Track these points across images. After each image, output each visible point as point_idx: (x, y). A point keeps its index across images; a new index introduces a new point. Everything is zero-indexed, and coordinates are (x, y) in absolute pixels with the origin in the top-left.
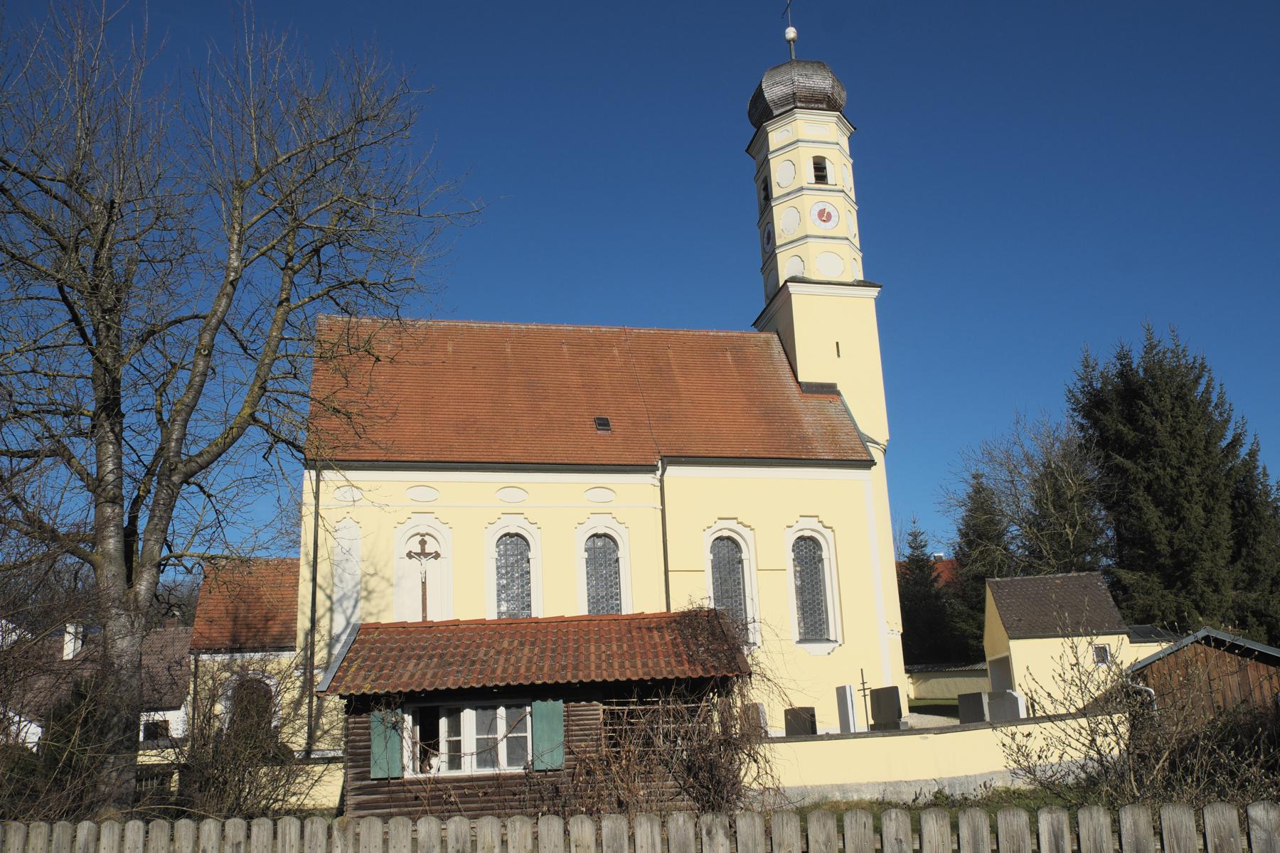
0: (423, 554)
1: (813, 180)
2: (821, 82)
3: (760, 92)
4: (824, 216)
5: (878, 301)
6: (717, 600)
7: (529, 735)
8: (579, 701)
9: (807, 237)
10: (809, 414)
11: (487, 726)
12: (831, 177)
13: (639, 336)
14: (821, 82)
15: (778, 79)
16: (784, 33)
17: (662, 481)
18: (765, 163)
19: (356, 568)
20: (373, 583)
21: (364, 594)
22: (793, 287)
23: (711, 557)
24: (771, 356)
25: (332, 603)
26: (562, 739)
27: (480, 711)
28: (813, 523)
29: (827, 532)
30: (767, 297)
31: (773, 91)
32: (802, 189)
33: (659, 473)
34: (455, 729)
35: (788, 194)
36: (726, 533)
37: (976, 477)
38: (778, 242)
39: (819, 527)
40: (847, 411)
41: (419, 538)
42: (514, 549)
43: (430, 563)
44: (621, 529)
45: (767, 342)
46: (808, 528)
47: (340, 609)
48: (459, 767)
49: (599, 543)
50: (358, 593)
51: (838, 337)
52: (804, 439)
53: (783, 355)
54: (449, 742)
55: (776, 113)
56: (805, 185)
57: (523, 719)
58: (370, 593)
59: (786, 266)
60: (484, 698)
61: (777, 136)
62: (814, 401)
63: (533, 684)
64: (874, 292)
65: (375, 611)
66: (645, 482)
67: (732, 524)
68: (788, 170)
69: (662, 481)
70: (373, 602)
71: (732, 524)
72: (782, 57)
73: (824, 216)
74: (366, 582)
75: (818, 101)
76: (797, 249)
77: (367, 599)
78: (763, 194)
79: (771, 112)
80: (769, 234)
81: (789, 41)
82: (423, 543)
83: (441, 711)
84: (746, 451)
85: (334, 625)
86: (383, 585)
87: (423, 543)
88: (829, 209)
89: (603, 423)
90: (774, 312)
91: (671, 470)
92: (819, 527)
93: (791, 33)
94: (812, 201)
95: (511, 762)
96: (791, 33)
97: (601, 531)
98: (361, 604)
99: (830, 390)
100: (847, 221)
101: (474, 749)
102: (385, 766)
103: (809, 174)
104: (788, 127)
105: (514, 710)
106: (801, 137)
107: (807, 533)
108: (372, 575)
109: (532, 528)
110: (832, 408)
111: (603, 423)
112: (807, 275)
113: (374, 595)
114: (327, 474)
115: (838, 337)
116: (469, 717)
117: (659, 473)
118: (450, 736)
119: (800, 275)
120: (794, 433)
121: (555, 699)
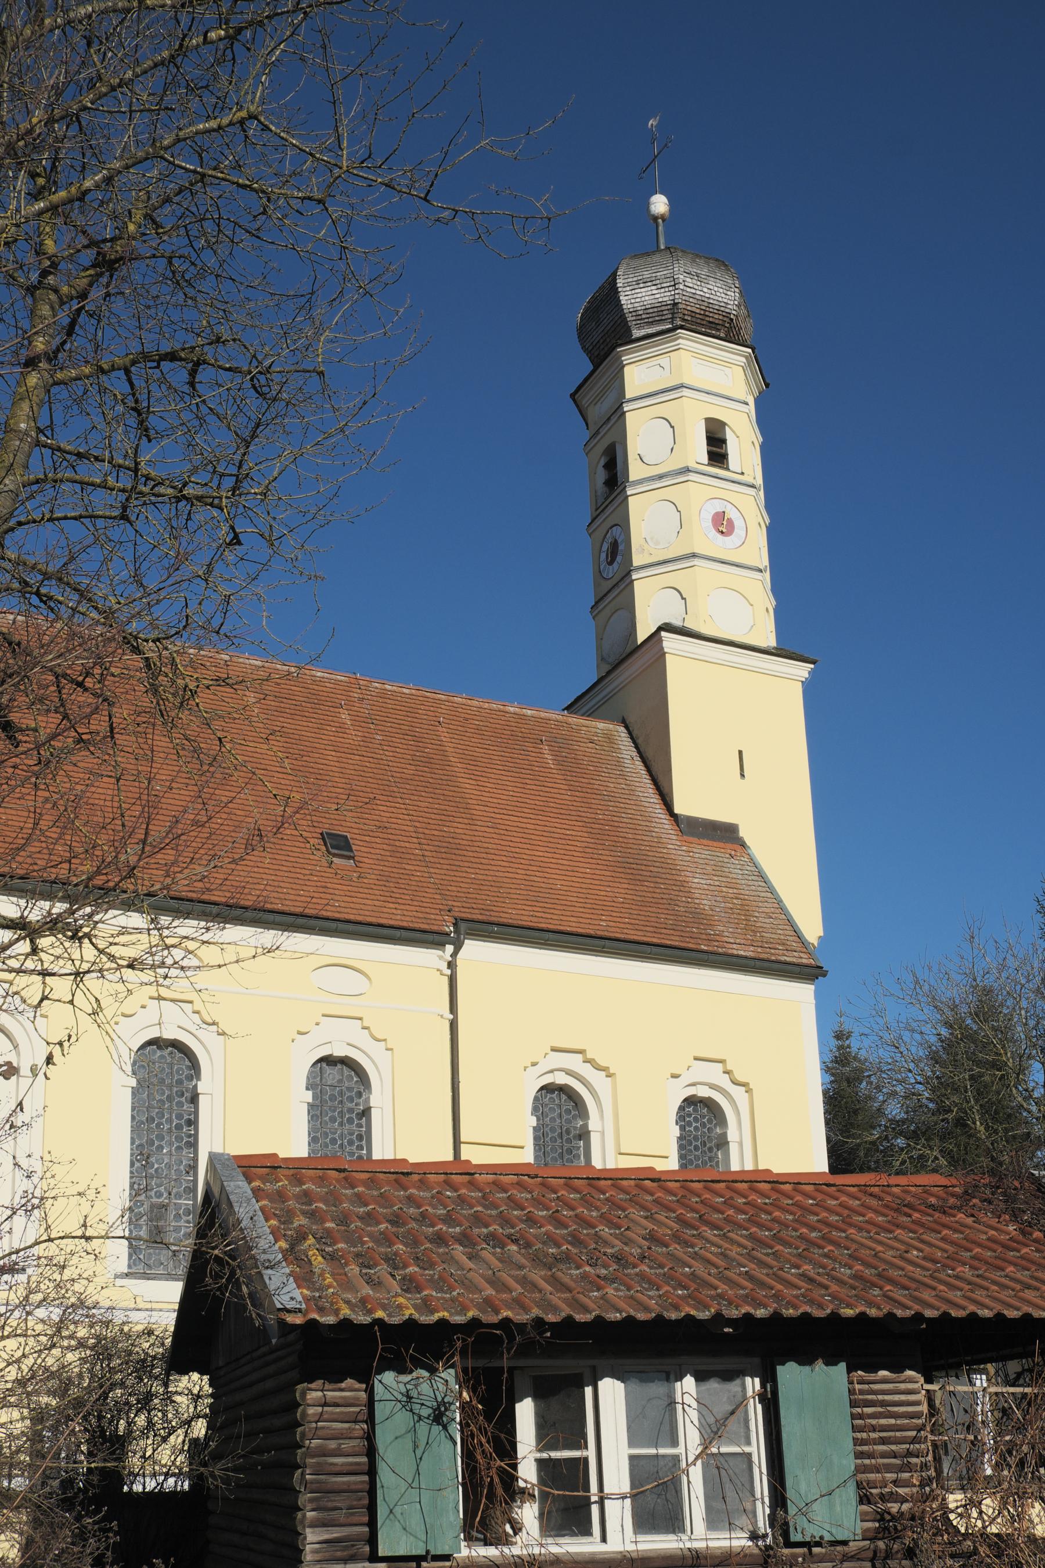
1: (705, 459)
2: (721, 292)
3: (609, 293)
4: (722, 524)
5: (809, 688)
7: (591, 1453)
8: (874, 1369)
9: (694, 555)
10: (697, 867)
11: (654, 1424)
12: (734, 459)
13: (383, 694)
14: (721, 292)
15: (646, 275)
16: (647, 205)
17: (451, 965)
18: (617, 415)
22: (670, 642)
23: (533, 1121)
24: (619, 763)
26: (850, 1463)
27: (635, 1386)
28: (714, 1074)
29: (738, 1092)
30: (602, 659)
31: (637, 295)
32: (687, 470)
33: (450, 949)
34: (565, 1425)
35: (661, 477)
36: (561, 1079)
37: (839, 1036)
38: (637, 560)
39: (724, 1082)
40: (762, 876)
42: (167, 1075)
44: (376, 1050)
45: (610, 738)
46: (705, 1079)
49: (332, 1074)
51: (741, 742)
52: (698, 916)
53: (639, 764)
54: (540, 1462)
55: (637, 333)
56: (692, 465)
57: (741, 1404)
59: (651, 605)
60: (652, 1348)
61: (640, 372)
62: (703, 852)
63: (834, 1317)
64: (803, 670)
66: (425, 962)
67: (574, 1062)
68: (653, 439)
69: (451, 965)
71: (574, 1062)
72: (647, 242)
73: (722, 524)
75: (713, 325)
76: (678, 577)
78: (601, 475)
79: (628, 331)
80: (615, 545)
81: (655, 218)
83: (521, 1381)
84: (603, 926)
86: (954, 975)
88: (732, 514)
89: (338, 844)
90: (624, 680)
91: (472, 948)
92: (724, 1082)
93: (659, 204)
94: (704, 495)
95: (713, 1521)
96: (659, 204)
97: (339, 1052)
99: (724, 834)
100: (752, 542)
101: (626, 1488)
102: (415, 1523)
103: (698, 451)
104: (664, 361)
105: (714, 1385)
106: (686, 381)
107: (703, 1092)
110: (735, 868)
111: (338, 844)
112: (690, 624)
115: (741, 742)
116: (611, 1398)
117: (450, 949)
118: (631, 1444)
119: (677, 623)
120: (669, 907)
121: (830, 1362)
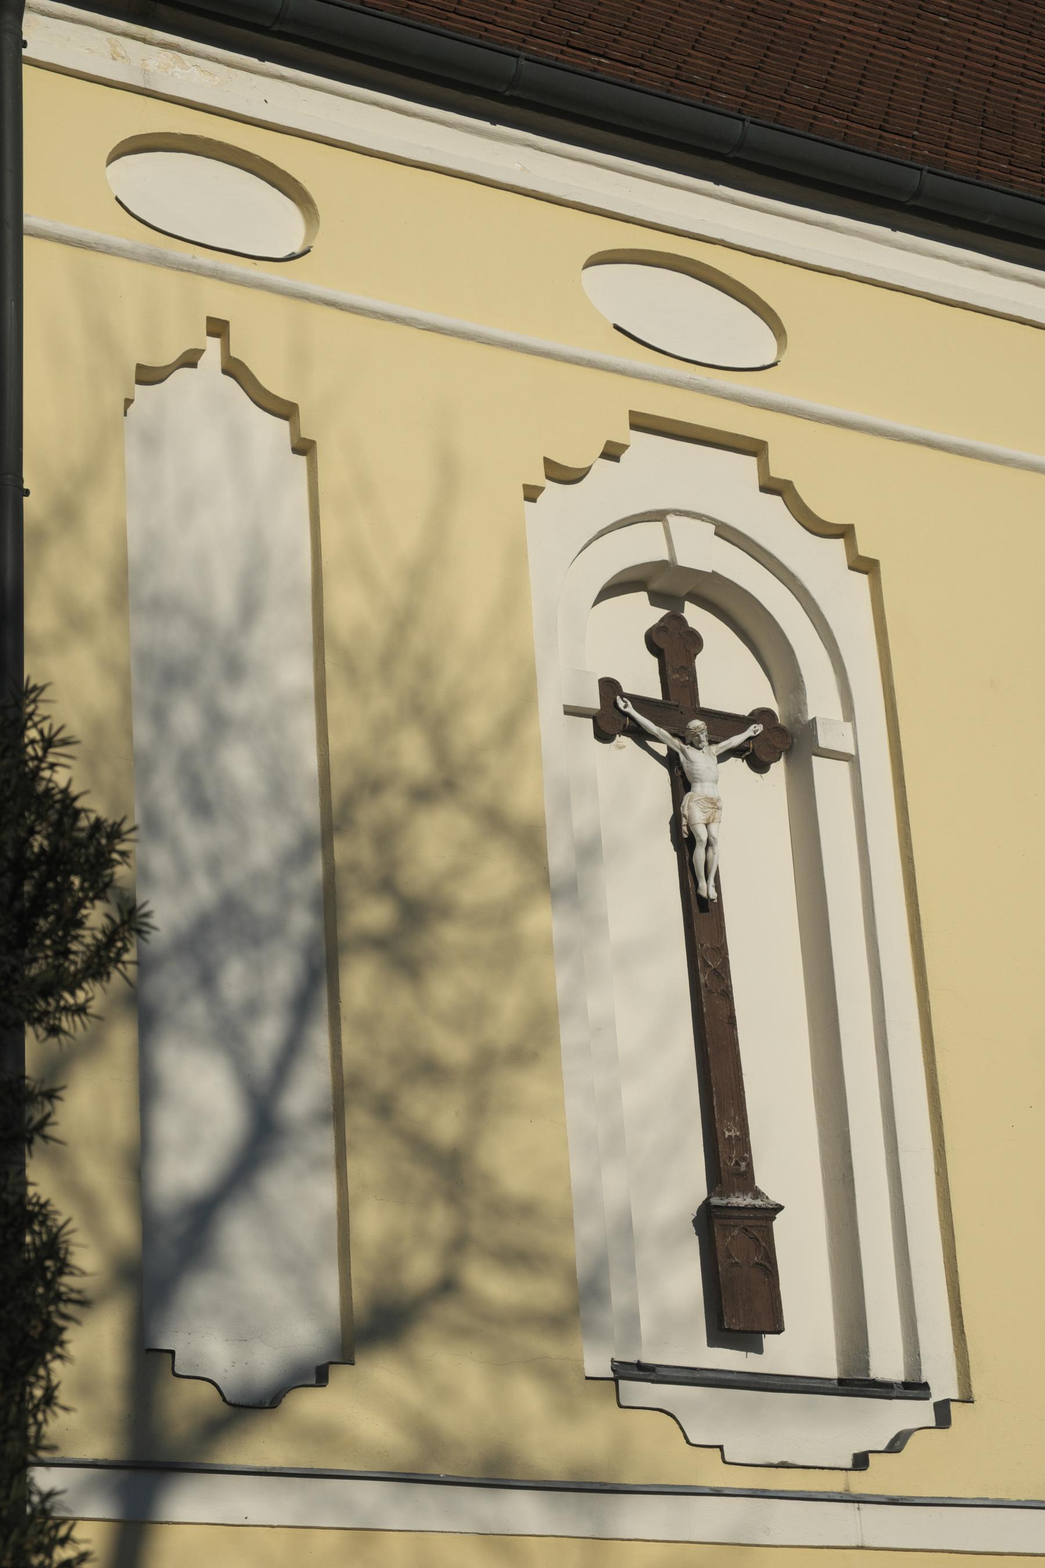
20: (435, 842)
47: (197, 1010)
58: (417, 913)
65: (454, 1049)
70: (446, 989)
85: (168, 1126)
108: (423, 795)
113: (451, 935)
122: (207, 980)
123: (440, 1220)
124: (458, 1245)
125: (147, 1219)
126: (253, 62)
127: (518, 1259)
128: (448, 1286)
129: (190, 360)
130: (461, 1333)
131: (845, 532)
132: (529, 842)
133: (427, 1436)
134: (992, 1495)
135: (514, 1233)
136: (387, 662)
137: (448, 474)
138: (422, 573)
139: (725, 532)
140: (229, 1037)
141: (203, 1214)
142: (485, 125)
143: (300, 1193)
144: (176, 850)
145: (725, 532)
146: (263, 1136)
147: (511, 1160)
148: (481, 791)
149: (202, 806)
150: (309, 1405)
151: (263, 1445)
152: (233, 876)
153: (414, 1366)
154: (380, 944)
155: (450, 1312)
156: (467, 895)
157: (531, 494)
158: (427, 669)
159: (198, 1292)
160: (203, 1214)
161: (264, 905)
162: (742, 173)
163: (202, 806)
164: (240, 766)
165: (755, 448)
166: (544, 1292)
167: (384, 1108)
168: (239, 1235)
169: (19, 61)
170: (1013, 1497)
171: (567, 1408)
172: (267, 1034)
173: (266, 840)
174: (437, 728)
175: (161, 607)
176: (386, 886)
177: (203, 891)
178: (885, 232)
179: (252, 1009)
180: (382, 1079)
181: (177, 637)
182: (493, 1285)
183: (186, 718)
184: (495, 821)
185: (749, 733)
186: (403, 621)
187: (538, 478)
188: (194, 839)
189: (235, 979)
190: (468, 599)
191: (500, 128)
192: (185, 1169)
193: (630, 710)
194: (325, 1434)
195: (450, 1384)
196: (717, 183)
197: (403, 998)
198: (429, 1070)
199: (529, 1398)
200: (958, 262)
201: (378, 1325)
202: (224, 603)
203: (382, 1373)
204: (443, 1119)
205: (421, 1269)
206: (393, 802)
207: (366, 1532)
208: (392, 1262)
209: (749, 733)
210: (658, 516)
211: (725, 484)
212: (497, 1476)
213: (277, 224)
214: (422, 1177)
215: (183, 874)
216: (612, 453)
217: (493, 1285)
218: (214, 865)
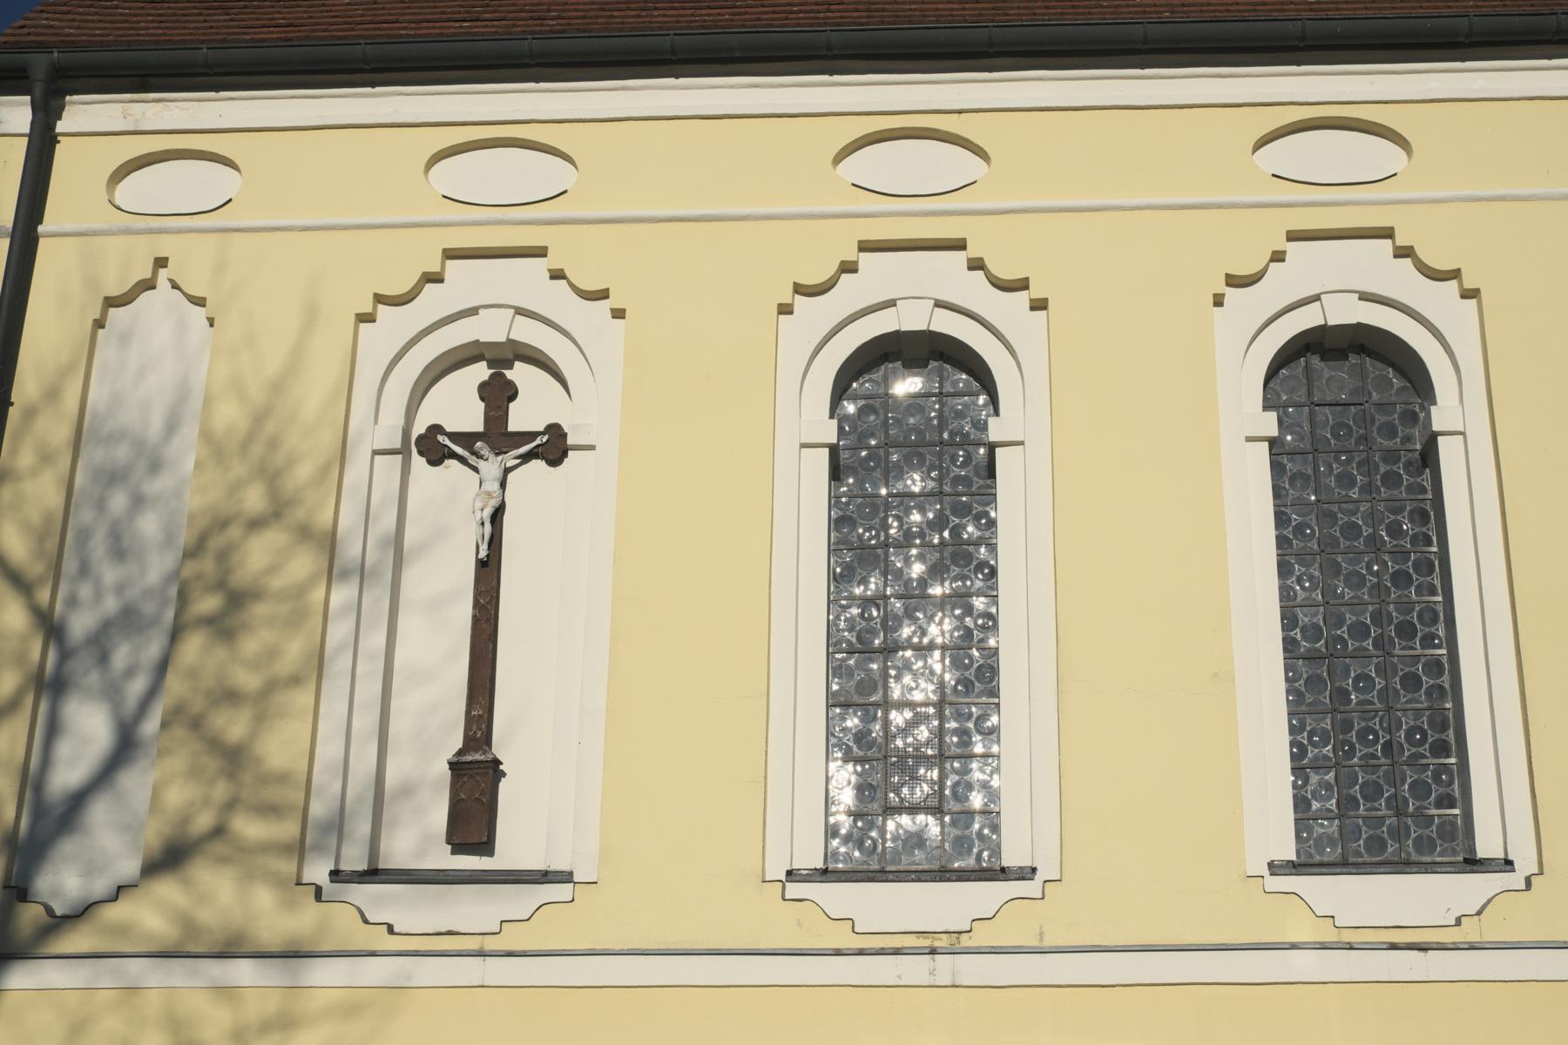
0: (496, 435)
6: (1298, 855)
19: (187, 485)
20: (257, 554)
21: (208, 604)
25: (65, 655)
41: (481, 371)
43: (532, 481)
47: (94, 678)
48: (485, 846)
49: (1336, 378)
50: (183, 598)
58: (238, 599)
65: (248, 680)
70: (250, 645)
74: (224, 556)
77: (223, 627)
82: (498, 394)
85: (64, 749)
87: (498, 394)
98: (193, 648)
108: (255, 524)
109: (1008, 310)
113: (260, 610)
114: (84, 114)
122: (104, 658)
123: (221, 791)
124: (231, 805)
125: (39, 810)
126: (212, 94)
127: (270, 810)
128: (218, 832)
129: (148, 285)
130: (224, 860)
131: (1455, 274)
132: (330, 543)
133: (189, 926)
134: (599, 947)
135: (272, 793)
136: (245, 446)
137: (311, 316)
138: (278, 387)
139: (1365, 297)
140: (112, 693)
141: (78, 800)
142: (369, 90)
143: (136, 782)
144: (98, 583)
145: (1365, 297)
146: (125, 748)
147: (279, 748)
148: (300, 514)
149: (119, 553)
150: (113, 913)
151: (77, 940)
152: (132, 594)
153: (187, 883)
154: (209, 621)
155: (218, 847)
156: (277, 583)
157: (1218, 301)
158: (273, 444)
159: (67, 847)
160: (78, 800)
161: (148, 608)
162: (640, 69)
163: (119, 553)
164: (149, 525)
165: (1388, 233)
166: (287, 829)
167: (196, 724)
168: (99, 812)
169: (30, 136)
170: (617, 947)
171: (290, 905)
172: (137, 687)
173: (157, 567)
174: (271, 476)
175: (114, 438)
176: (220, 585)
177: (111, 605)
178: (671, 81)
179: (130, 673)
180: (198, 705)
181: (122, 453)
182: (250, 828)
183: (118, 501)
184: (305, 533)
185: (538, 442)
186: (260, 418)
187: (1221, 287)
188: (110, 575)
189: (121, 656)
190: (315, 390)
191: (379, 89)
192: (68, 774)
193: (447, 442)
194: (122, 930)
195: (215, 893)
196: (537, 81)
197: (221, 653)
198: (230, 696)
199: (264, 898)
200: (732, 87)
201: (170, 858)
202: (156, 425)
203: (167, 889)
204: (234, 726)
205: (204, 821)
206: (235, 532)
207: (133, 989)
208: (185, 819)
209: (538, 442)
210: (1317, 298)
211: (1372, 265)
212: (228, 951)
213: (961, 164)
214: (212, 764)
215: (98, 595)
216: (1278, 257)
217: (250, 828)
218: (120, 589)
